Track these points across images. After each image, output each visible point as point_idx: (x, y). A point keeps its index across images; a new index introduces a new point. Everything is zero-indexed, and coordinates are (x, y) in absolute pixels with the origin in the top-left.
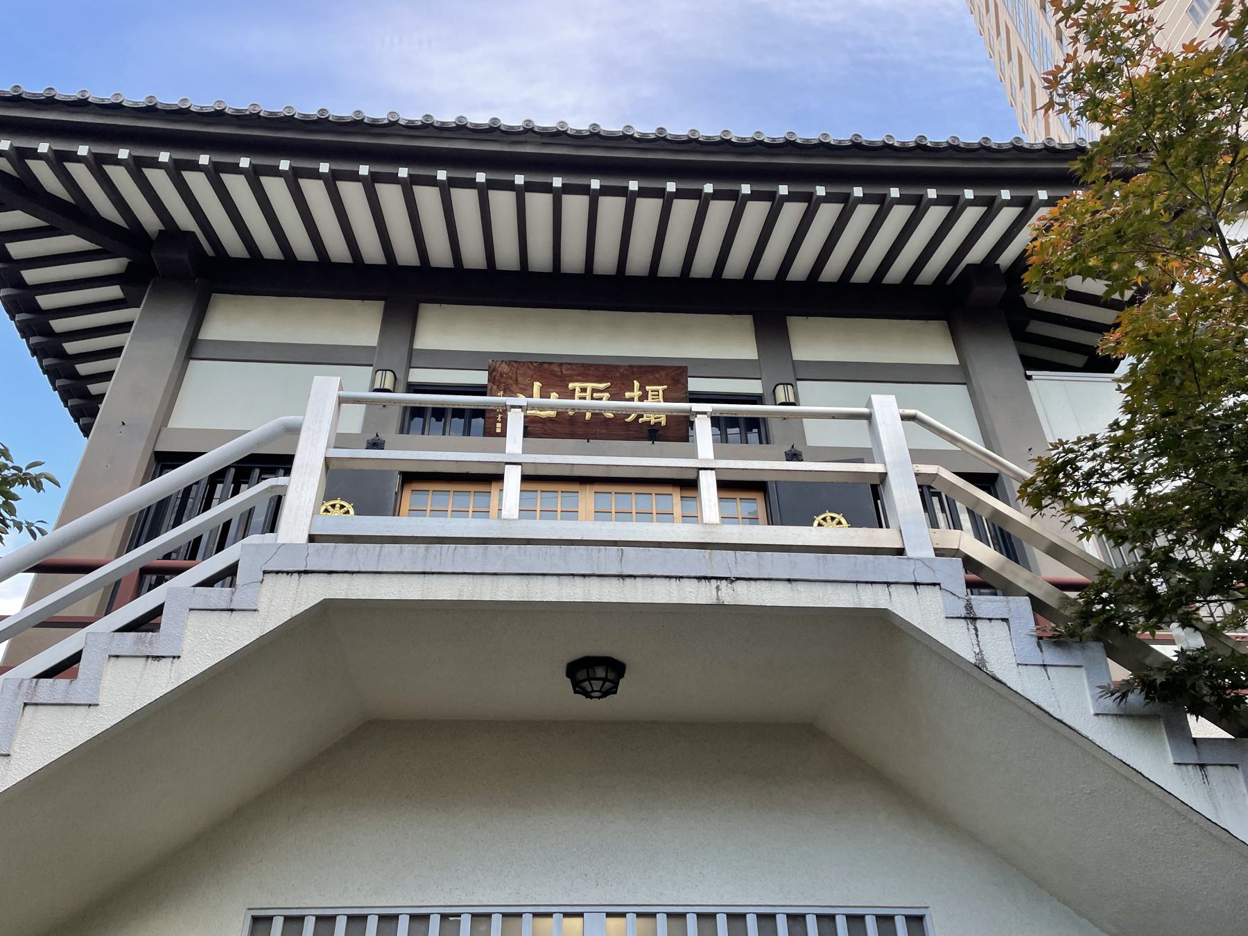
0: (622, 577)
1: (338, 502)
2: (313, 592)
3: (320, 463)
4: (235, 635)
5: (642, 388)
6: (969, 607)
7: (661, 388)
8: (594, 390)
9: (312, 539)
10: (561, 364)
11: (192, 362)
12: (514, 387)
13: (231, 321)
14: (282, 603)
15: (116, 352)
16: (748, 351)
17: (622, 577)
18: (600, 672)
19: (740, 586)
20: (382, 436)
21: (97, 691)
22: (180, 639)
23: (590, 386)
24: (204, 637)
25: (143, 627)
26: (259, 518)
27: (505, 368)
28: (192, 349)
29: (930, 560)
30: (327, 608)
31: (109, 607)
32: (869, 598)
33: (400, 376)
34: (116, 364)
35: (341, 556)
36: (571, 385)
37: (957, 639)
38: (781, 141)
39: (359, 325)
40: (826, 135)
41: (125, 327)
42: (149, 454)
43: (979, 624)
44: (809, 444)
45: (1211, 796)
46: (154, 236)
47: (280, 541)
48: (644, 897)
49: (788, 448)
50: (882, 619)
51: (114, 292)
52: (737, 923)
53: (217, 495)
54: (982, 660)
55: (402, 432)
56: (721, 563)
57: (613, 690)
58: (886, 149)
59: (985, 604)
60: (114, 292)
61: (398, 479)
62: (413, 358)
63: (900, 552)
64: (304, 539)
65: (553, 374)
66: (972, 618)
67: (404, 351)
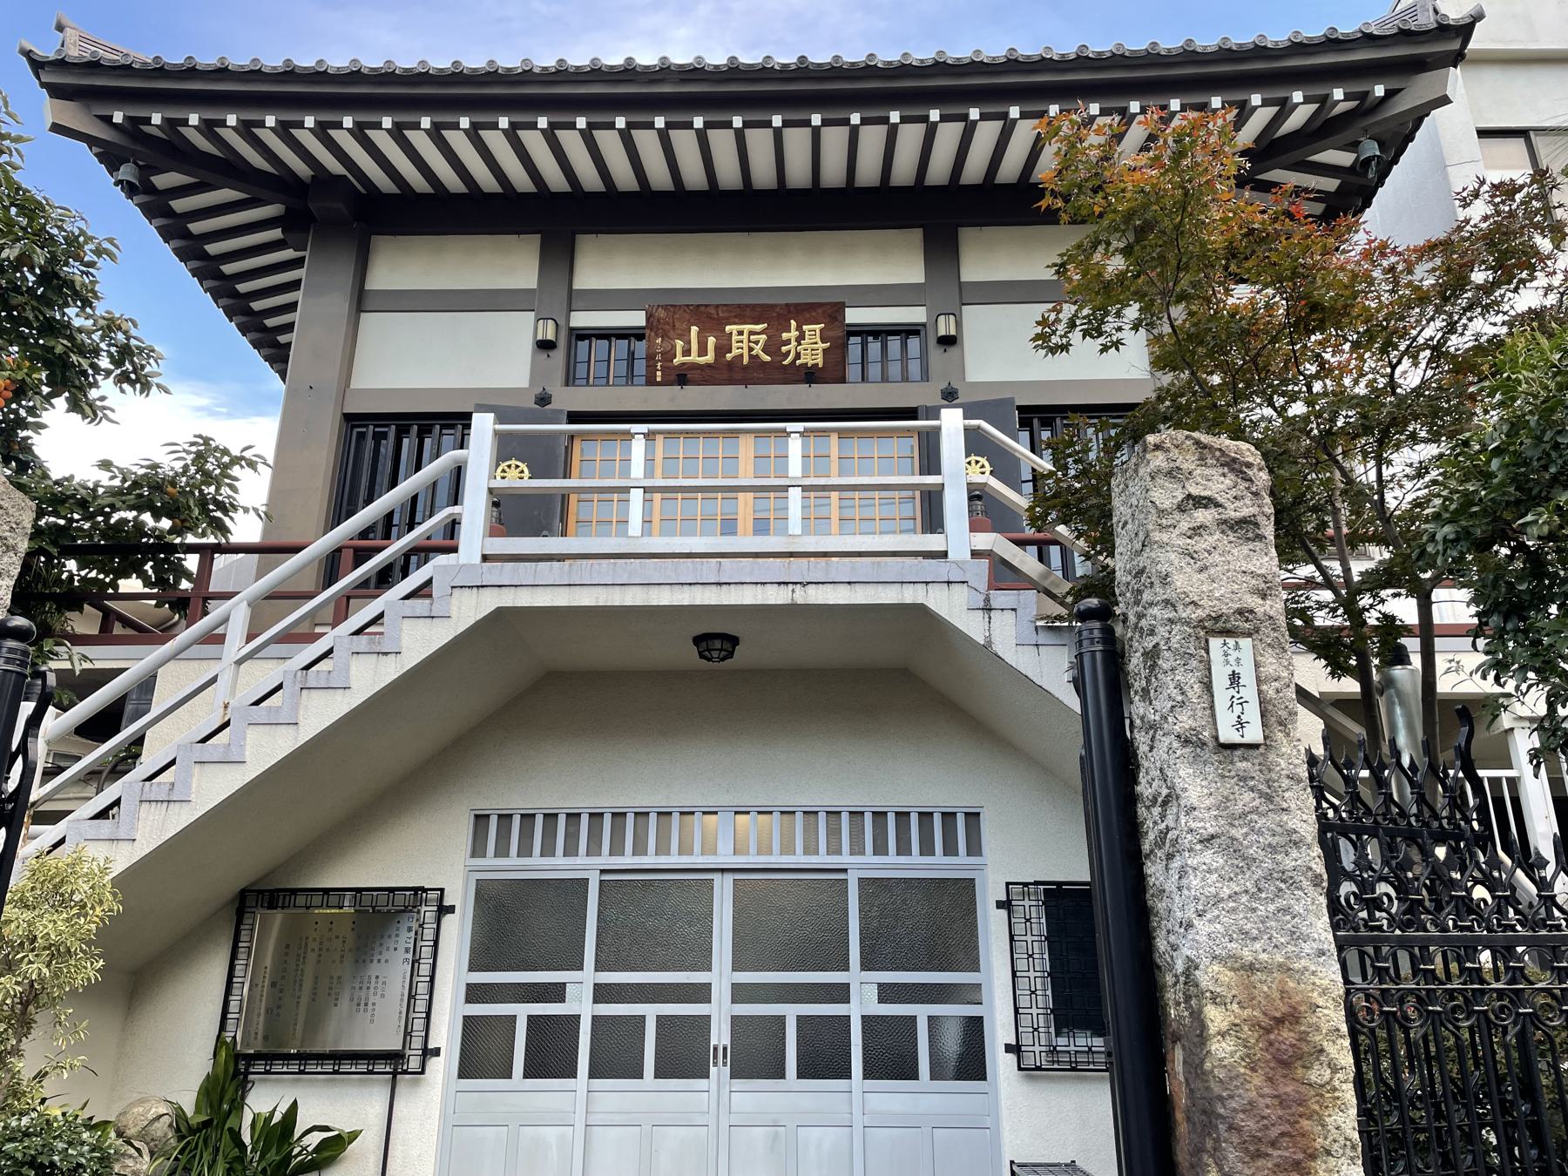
0: (720, 584)
1: (513, 462)
2: (489, 602)
4: (437, 636)
5: (799, 328)
6: (987, 600)
7: (818, 327)
8: (751, 333)
9: (485, 558)
11: (363, 315)
12: (671, 334)
13: (399, 266)
14: (467, 611)
15: (291, 307)
16: (911, 271)
17: (720, 584)
18: (718, 644)
19: (811, 589)
20: (549, 390)
21: (348, 678)
22: (399, 639)
23: (747, 328)
24: (418, 640)
25: (231, 157)
26: (443, 493)
27: (662, 313)
28: (362, 301)
29: (964, 562)
30: (500, 614)
31: (330, 580)
32: (910, 595)
33: (562, 322)
34: (295, 317)
35: (507, 572)
36: (728, 328)
37: (972, 626)
38: (930, 62)
39: (514, 265)
40: (978, 52)
41: (295, 285)
42: (339, 416)
43: (993, 613)
44: (969, 379)
46: (309, 181)
47: (462, 561)
48: (763, 801)
49: (944, 385)
50: (920, 610)
51: (276, 234)
52: (880, 819)
53: (412, 566)
54: (990, 643)
55: (567, 385)
56: (798, 569)
57: (730, 655)
58: (1043, 64)
59: (1000, 598)
60: (276, 234)
62: (574, 299)
63: (944, 555)
64: (478, 559)
65: (709, 316)
66: (988, 609)
67: (565, 294)
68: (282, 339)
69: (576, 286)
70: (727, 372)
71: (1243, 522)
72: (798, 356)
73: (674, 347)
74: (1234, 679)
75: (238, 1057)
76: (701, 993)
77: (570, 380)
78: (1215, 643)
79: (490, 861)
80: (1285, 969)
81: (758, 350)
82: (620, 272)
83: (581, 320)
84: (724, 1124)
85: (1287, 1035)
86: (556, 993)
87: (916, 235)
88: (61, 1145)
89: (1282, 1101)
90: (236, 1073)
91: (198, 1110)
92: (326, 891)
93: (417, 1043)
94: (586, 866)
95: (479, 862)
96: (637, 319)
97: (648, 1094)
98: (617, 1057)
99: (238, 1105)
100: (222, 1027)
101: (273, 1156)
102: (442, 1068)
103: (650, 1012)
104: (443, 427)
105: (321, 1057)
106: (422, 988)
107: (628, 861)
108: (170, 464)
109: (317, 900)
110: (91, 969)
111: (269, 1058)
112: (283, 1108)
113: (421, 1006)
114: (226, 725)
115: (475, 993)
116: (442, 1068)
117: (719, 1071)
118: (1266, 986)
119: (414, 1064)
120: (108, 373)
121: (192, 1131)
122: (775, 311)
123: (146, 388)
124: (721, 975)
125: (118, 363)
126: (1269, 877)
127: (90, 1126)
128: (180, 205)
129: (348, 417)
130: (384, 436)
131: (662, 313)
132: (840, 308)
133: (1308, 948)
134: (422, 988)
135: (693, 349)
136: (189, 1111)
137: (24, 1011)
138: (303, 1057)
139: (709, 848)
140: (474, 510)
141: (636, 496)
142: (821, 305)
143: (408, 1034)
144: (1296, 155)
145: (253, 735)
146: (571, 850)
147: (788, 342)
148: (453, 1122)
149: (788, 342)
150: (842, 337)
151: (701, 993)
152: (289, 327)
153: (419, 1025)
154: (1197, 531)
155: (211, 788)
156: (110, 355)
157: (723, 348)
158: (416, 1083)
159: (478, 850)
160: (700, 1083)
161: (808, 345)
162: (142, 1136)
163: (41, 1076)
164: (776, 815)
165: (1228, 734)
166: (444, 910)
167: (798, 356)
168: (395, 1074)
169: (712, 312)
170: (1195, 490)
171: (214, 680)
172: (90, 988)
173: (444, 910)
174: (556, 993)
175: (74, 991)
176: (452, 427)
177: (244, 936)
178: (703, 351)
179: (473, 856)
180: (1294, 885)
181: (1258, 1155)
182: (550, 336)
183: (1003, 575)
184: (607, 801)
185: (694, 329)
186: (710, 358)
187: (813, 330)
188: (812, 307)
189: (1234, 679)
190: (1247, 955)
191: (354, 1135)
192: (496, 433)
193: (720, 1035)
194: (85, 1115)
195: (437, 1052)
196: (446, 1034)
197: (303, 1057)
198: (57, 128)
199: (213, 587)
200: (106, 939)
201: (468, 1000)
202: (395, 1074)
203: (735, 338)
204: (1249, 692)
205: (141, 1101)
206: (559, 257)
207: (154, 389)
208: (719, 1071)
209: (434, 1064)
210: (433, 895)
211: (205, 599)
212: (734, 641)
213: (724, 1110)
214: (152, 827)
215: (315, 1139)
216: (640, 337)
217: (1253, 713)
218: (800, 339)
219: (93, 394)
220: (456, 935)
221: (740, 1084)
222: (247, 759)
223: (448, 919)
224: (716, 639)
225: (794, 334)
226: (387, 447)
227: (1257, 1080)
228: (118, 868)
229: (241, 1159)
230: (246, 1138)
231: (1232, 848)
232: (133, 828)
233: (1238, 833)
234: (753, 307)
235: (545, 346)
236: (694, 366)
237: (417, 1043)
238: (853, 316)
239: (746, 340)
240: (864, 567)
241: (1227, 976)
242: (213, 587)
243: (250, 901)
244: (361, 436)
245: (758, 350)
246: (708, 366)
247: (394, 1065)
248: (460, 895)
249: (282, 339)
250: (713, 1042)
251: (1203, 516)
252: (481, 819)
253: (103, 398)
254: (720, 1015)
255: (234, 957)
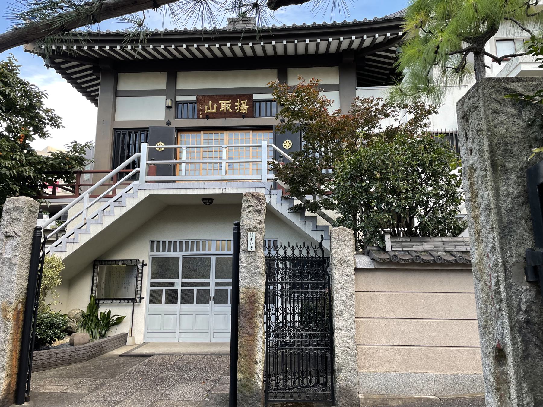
3: (145, 164)
5: (240, 102)
6: (270, 192)
8: (227, 103)
10: (217, 95)
13: (126, 83)
14: (142, 195)
20: (170, 121)
21: (114, 212)
27: (201, 98)
28: (117, 94)
30: (150, 196)
33: (173, 100)
35: (151, 185)
39: (159, 82)
41: (98, 84)
45: (305, 226)
51: (91, 72)
59: (273, 191)
60: (91, 72)
61: (174, 132)
62: (177, 92)
66: (270, 194)
68: (96, 98)
69: (178, 88)
70: (220, 115)
71: (258, 210)
72: (240, 110)
73: (205, 107)
74: (252, 239)
75: (96, 299)
76: (208, 284)
77: (176, 117)
78: (249, 233)
79: (155, 253)
80: (254, 288)
81: (228, 108)
82: (191, 83)
83: (179, 98)
84: (213, 314)
85: (253, 299)
86: (172, 284)
87: (275, 71)
88: (55, 319)
89: (250, 309)
90: (96, 303)
91: (87, 311)
92: (115, 261)
93: (138, 296)
94: (179, 254)
95: (152, 253)
96: (194, 98)
97: (194, 307)
98: (187, 298)
99: (97, 310)
100: (92, 293)
101: (105, 321)
102: (145, 302)
103: (195, 289)
104: (141, 131)
105: (124, 299)
106: (139, 283)
107: (189, 253)
108: (65, 150)
109: (113, 263)
110: (59, 281)
111: (104, 299)
112: (108, 311)
113: (139, 287)
114: (86, 224)
115: (152, 284)
116: (145, 302)
117: (212, 302)
118: (250, 291)
119: (138, 301)
120: (48, 124)
121: (86, 316)
122: (234, 96)
123: (59, 127)
124: (212, 280)
125: (50, 121)
126: (253, 273)
127: (61, 315)
128: (63, 66)
129: (115, 129)
130: (125, 134)
131: (201, 98)
132: (252, 96)
133: (258, 285)
134: (139, 283)
135: (210, 108)
136: (85, 312)
137: (44, 291)
138: (112, 300)
139: (209, 250)
140: (142, 169)
141: (184, 165)
142: (246, 95)
143: (136, 294)
144: (385, 48)
145: (92, 227)
146: (175, 250)
147: (237, 106)
148: (148, 315)
149: (237, 106)
150: (252, 103)
151: (208, 284)
152: (97, 95)
153: (139, 292)
154: (249, 212)
155: (83, 239)
156: (48, 119)
157: (219, 108)
158: (139, 305)
159: (152, 250)
160: (207, 305)
161: (243, 107)
162: (74, 318)
163: (49, 305)
164: (226, 241)
165: (249, 249)
166: (144, 265)
167: (240, 110)
168: (134, 303)
169: (216, 96)
170: (250, 204)
171: (82, 213)
172: (59, 286)
173: (144, 265)
174: (172, 284)
175: (55, 286)
176: (144, 131)
177: (95, 271)
178: (213, 109)
179: (151, 252)
180: (257, 274)
181: (245, 317)
182: (170, 105)
183: (275, 186)
184: (184, 238)
185: (210, 102)
186: (215, 111)
187: (244, 102)
188: (244, 95)
189: (252, 239)
190: (248, 286)
191: (124, 317)
192: (148, 148)
193: (212, 294)
194: (60, 313)
195: (144, 298)
196: (145, 293)
197: (112, 300)
198: (26, 51)
199: (81, 183)
200: (62, 273)
201: (151, 286)
202: (134, 303)
203: (222, 105)
204: (254, 242)
205: (73, 310)
206: (172, 79)
207: (61, 127)
208: (212, 302)
209: (143, 301)
210: (141, 262)
211: (79, 186)
212: (212, 200)
213: (213, 312)
214: (71, 249)
215: (115, 318)
216: (195, 103)
217: (254, 246)
218: (241, 105)
219: (45, 130)
220: (147, 271)
221: (217, 305)
222: (91, 232)
223: (145, 267)
224: (208, 200)
225: (239, 103)
226: (127, 136)
227: (247, 305)
228: (63, 258)
229: (98, 322)
230: (99, 318)
231: (248, 268)
232: (66, 249)
233: (249, 266)
234: (227, 95)
235: (168, 107)
236: (211, 113)
237: (138, 296)
238: (256, 97)
239: (225, 105)
240: (240, 184)
241: (245, 289)
242: (81, 183)
243: (96, 263)
244: (119, 134)
245: (228, 108)
246: (215, 113)
247: (133, 301)
248: (148, 261)
249: (96, 98)
250: (210, 295)
251: (251, 209)
252: (152, 243)
253: (47, 131)
254: (212, 290)
255: (93, 276)
